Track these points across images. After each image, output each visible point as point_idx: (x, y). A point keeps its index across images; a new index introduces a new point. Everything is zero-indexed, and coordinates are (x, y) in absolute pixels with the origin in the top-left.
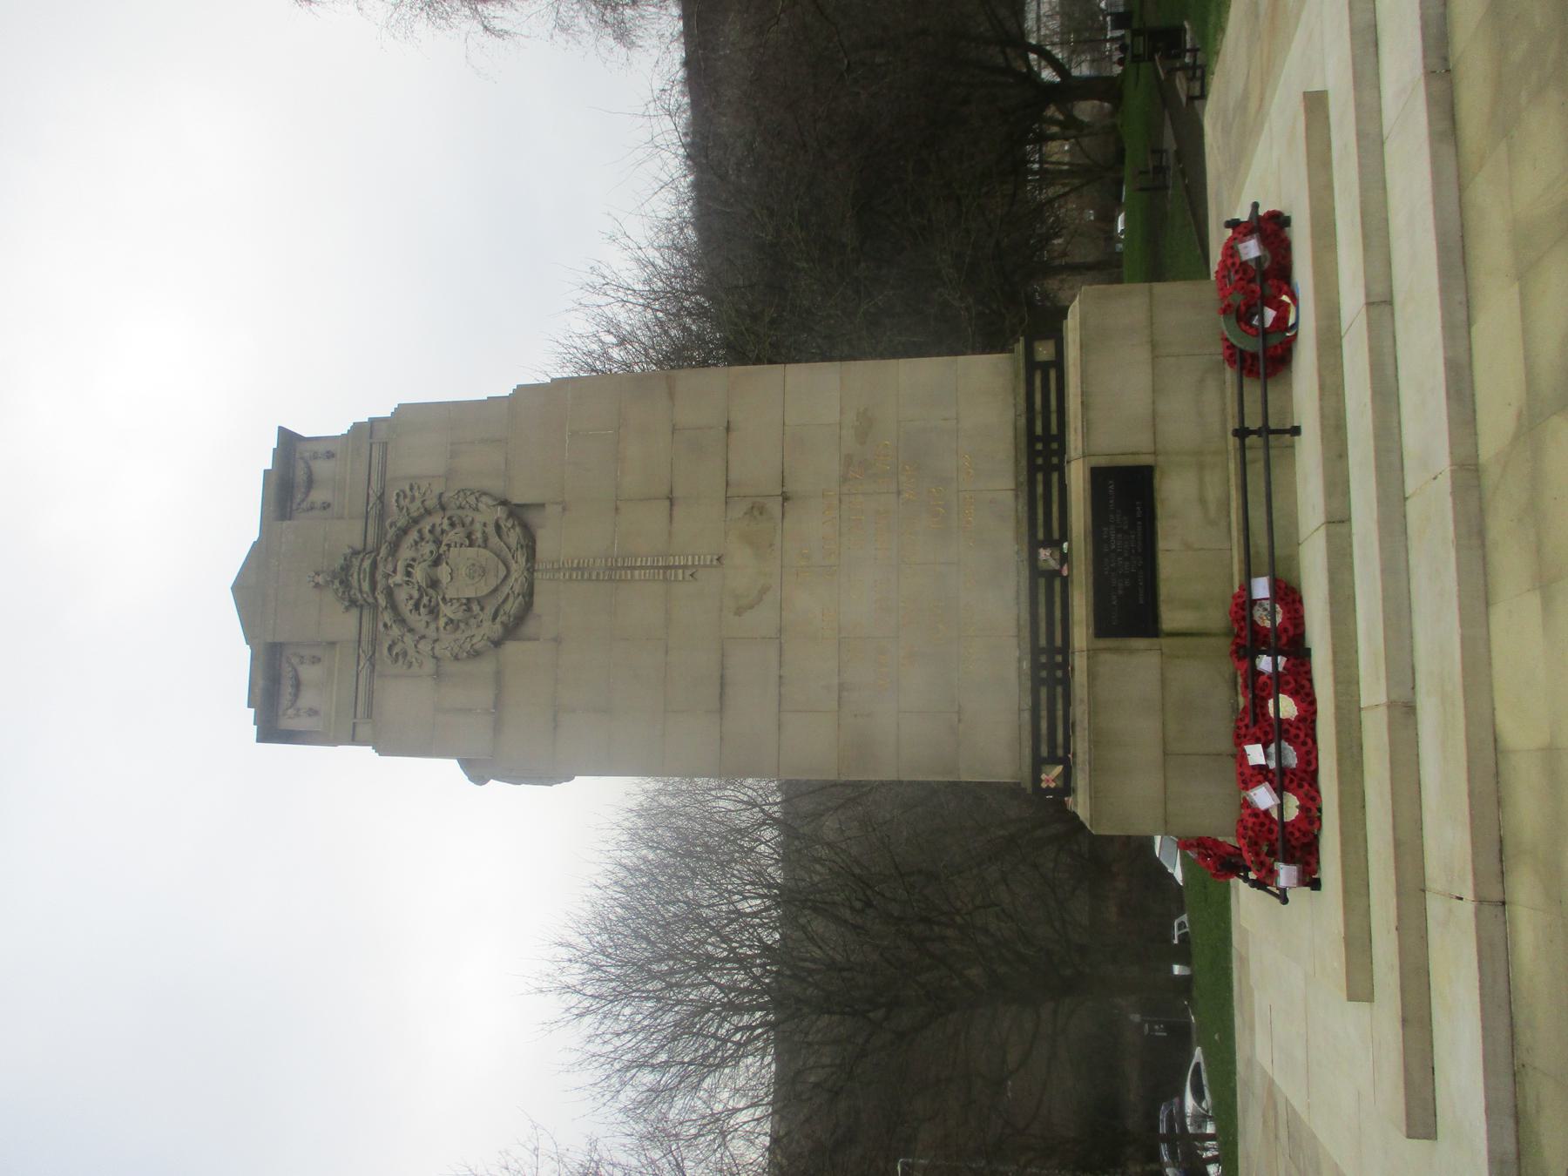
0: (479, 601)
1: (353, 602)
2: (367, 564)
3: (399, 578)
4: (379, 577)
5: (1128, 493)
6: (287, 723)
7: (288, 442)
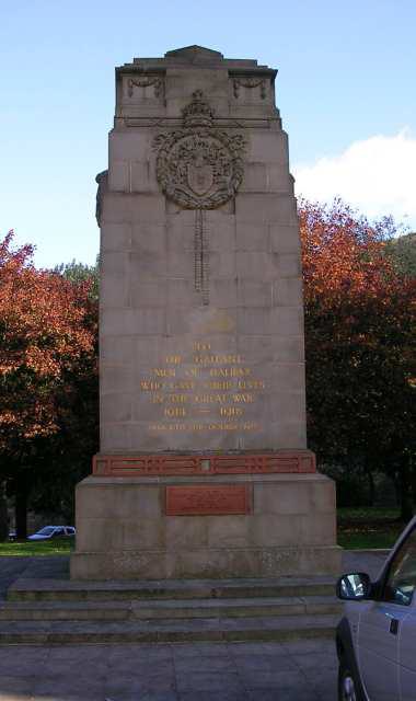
0: (186, 181)
1: (186, 115)
2: (205, 122)
3: (198, 139)
4: (199, 128)
5: (241, 505)
6: (125, 80)
7: (272, 74)
